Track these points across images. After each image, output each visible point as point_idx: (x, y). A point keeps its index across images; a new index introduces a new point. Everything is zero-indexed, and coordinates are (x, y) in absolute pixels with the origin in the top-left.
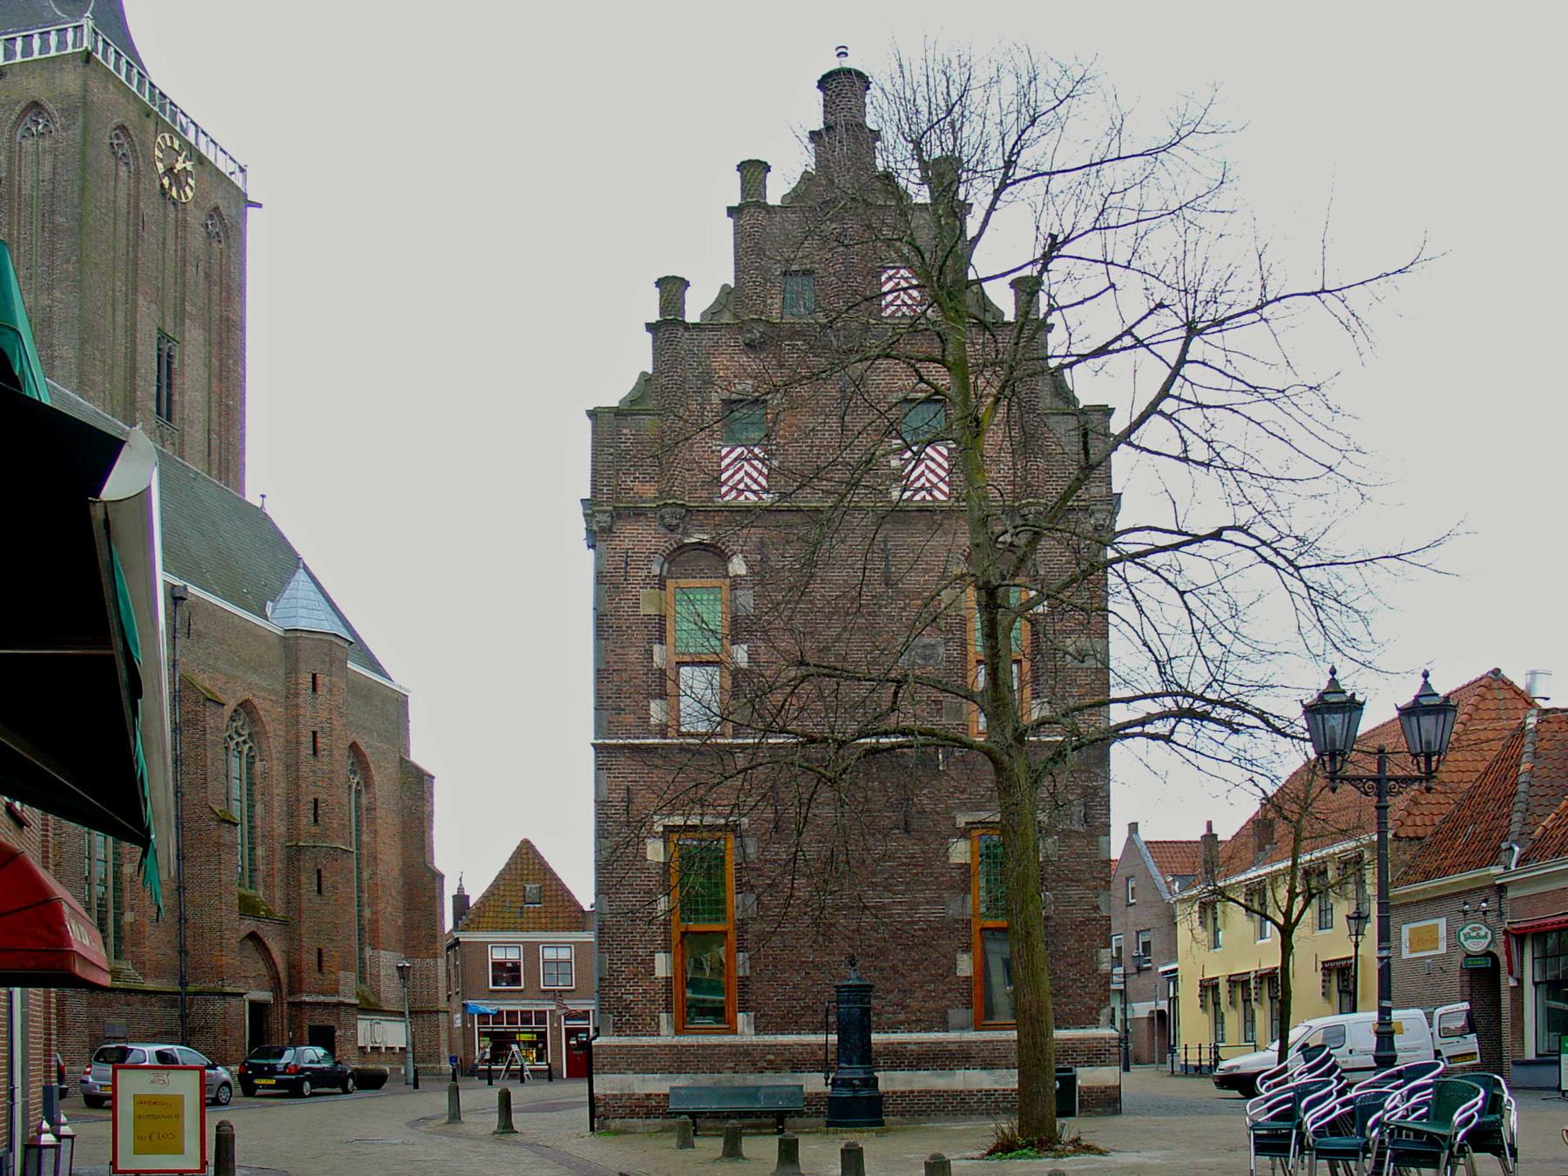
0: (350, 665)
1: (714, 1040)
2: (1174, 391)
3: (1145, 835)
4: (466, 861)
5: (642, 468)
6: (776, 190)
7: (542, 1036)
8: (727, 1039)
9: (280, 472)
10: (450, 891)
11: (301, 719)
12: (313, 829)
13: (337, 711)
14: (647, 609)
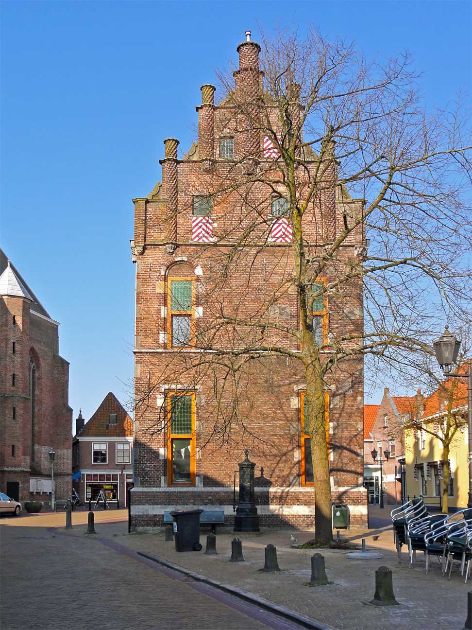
0: (31, 311)
1: (185, 489)
2: (387, 196)
3: (392, 394)
4: (83, 404)
7: (115, 486)
8: (190, 489)
10: (75, 417)
11: (8, 337)
12: (12, 388)
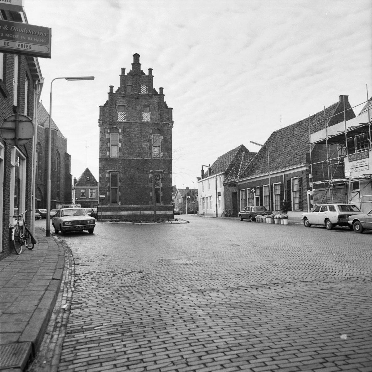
5: (107, 113)
6: (127, 72)
9: (65, 137)
13: (53, 141)
14: (107, 137)
